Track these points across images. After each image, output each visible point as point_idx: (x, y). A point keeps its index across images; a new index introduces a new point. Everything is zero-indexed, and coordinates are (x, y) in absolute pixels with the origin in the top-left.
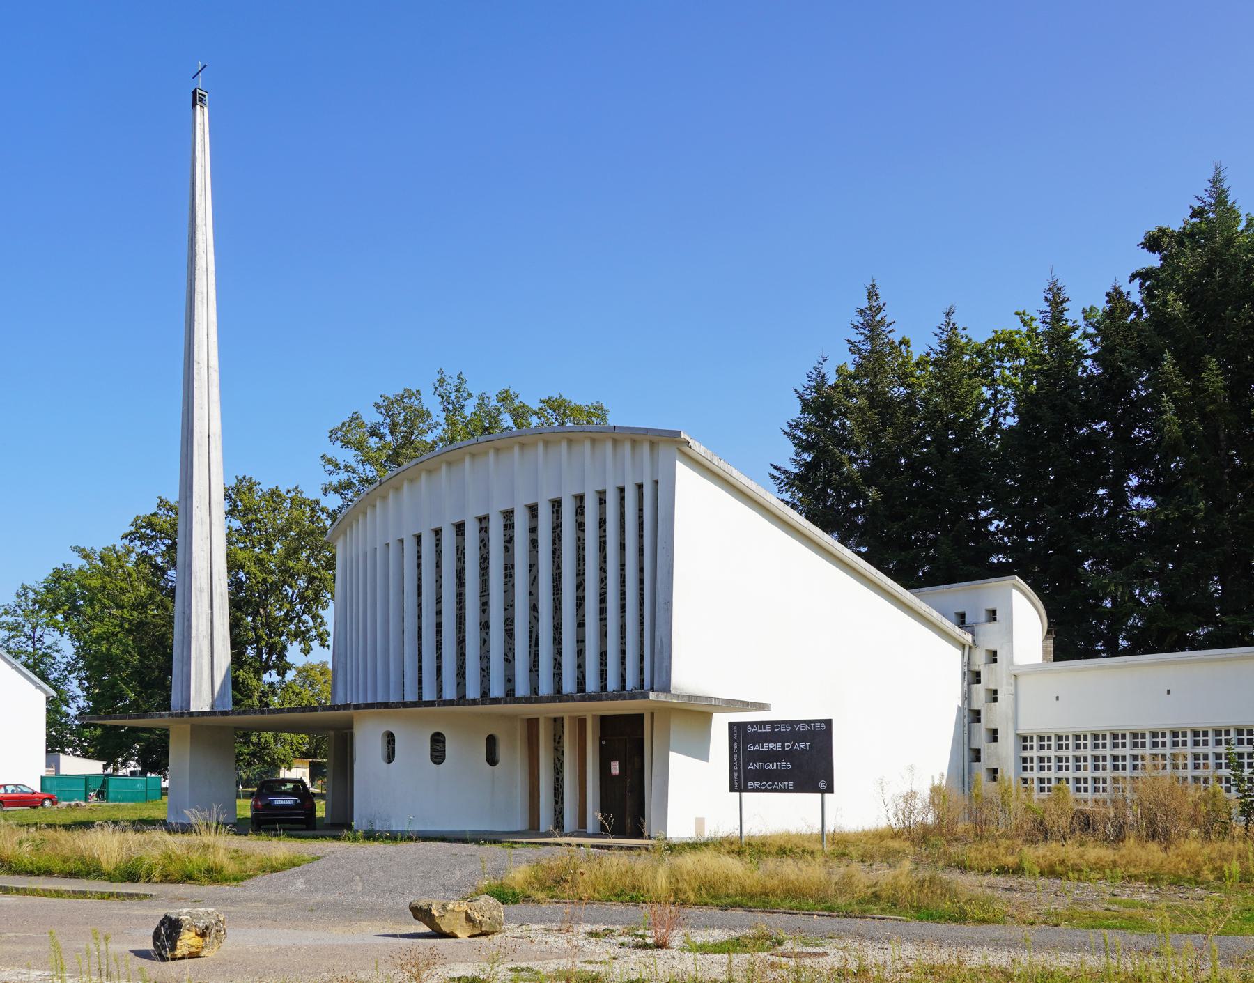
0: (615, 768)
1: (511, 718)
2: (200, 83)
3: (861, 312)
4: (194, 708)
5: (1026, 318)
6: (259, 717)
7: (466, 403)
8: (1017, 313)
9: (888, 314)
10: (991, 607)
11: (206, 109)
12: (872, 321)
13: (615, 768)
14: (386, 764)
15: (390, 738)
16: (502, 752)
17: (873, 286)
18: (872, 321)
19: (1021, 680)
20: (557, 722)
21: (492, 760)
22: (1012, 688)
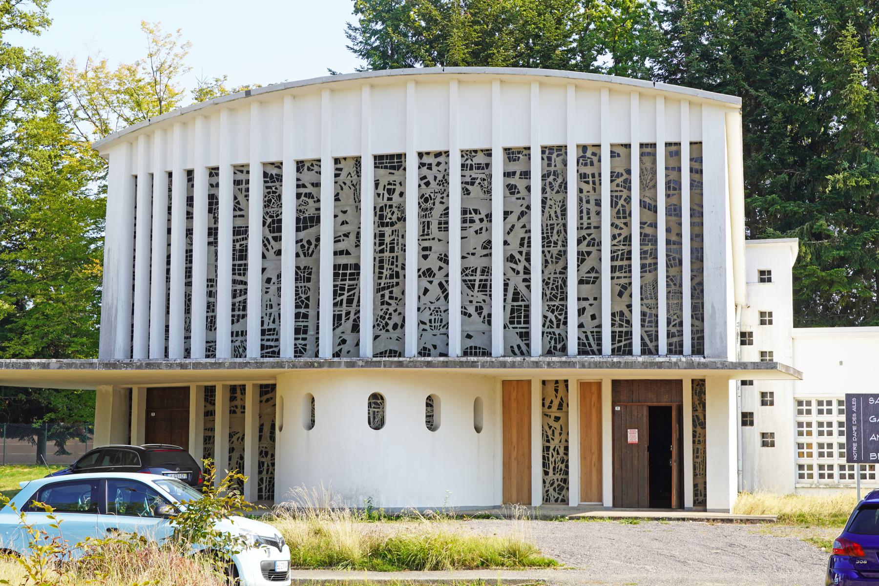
15: (376, 401)
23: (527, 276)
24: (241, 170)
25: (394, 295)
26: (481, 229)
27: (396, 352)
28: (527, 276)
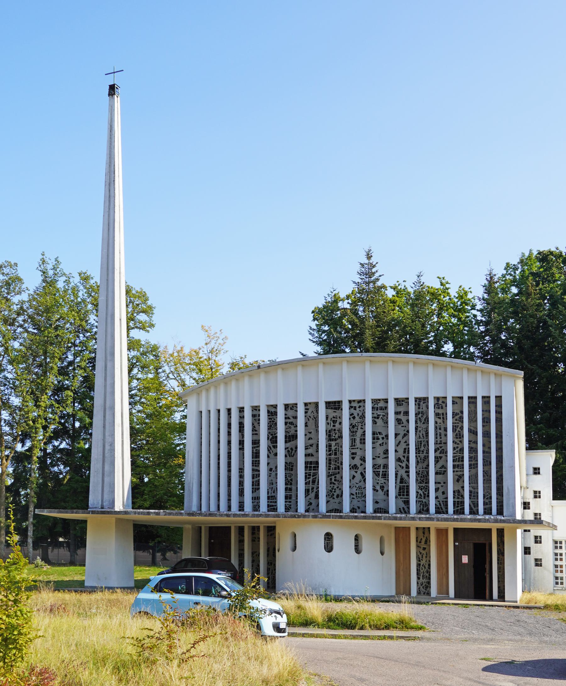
0: (465, 559)
1: (389, 526)
2: (117, 80)
3: (362, 265)
4: (117, 509)
5: (443, 281)
6: (226, 518)
7: (60, 279)
8: (438, 278)
9: (379, 270)
10: (536, 466)
11: (119, 98)
12: (368, 271)
13: (465, 559)
14: (291, 552)
15: (328, 537)
16: (365, 545)
17: (370, 250)
18: (368, 271)
19: (554, 508)
20: (426, 531)
21: (358, 550)
22: (551, 513)
23: (407, 470)
24: (256, 409)
25: (337, 479)
26: (383, 443)
27: (338, 510)
28: (407, 470)
